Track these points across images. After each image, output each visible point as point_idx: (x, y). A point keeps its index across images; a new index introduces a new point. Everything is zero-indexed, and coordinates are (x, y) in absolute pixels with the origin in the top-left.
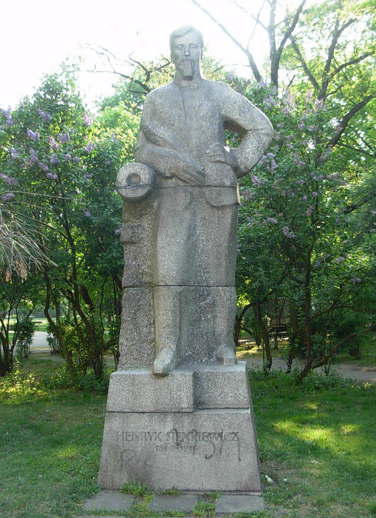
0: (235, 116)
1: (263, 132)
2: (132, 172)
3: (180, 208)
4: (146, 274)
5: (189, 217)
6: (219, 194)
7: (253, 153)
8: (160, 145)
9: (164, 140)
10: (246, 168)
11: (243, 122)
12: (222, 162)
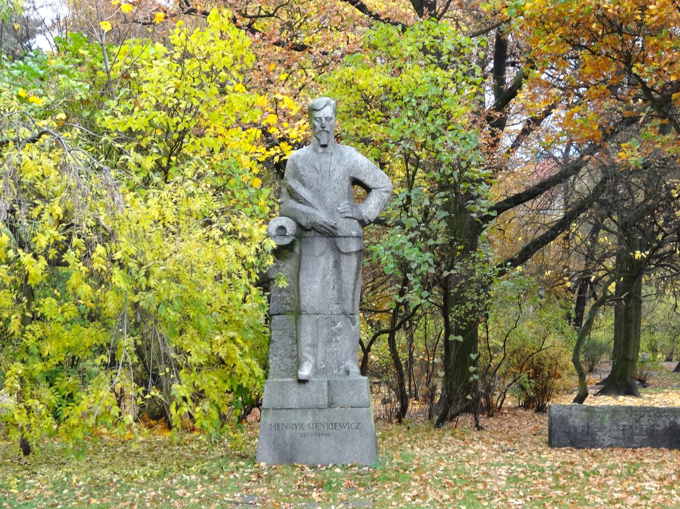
0: (361, 177)
1: (384, 189)
2: (280, 225)
3: (317, 254)
4: (289, 304)
5: (324, 261)
6: (347, 243)
7: (376, 208)
8: (301, 203)
9: (305, 199)
10: (369, 220)
11: (368, 181)
12: (350, 218)
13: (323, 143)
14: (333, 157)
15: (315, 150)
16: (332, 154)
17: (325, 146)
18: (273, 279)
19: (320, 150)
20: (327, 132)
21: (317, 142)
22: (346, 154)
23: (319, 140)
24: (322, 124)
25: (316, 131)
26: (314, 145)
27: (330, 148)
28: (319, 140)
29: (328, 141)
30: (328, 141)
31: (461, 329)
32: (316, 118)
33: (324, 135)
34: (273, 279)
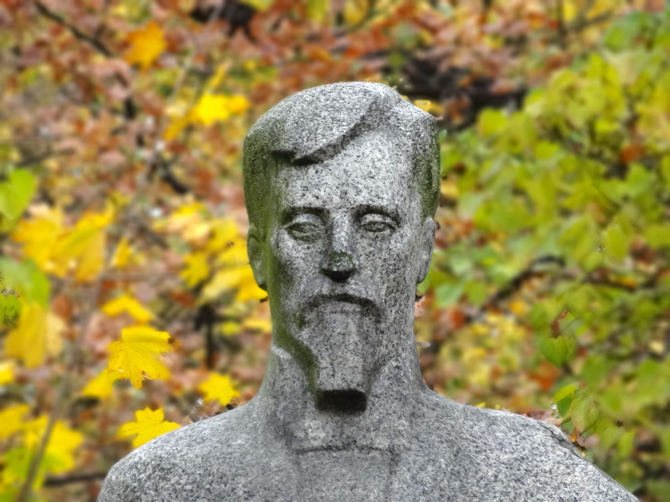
13: (331, 380)
14: (404, 474)
15: (284, 432)
16: (394, 457)
17: (346, 403)
18: (231, 33)
19: (316, 428)
20: (366, 305)
21: (293, 377)
22: (493, 462)
23: (306, 360)
24: (330, 254)
25: (293, 303)
26: (276, 395)
27: (382, 422)
28: (306, 360)
29: (373, 371)
30: (373, 371)
31: (261, 266)
32: (289, 215)
33: (345, 323)
34: (231, 33)
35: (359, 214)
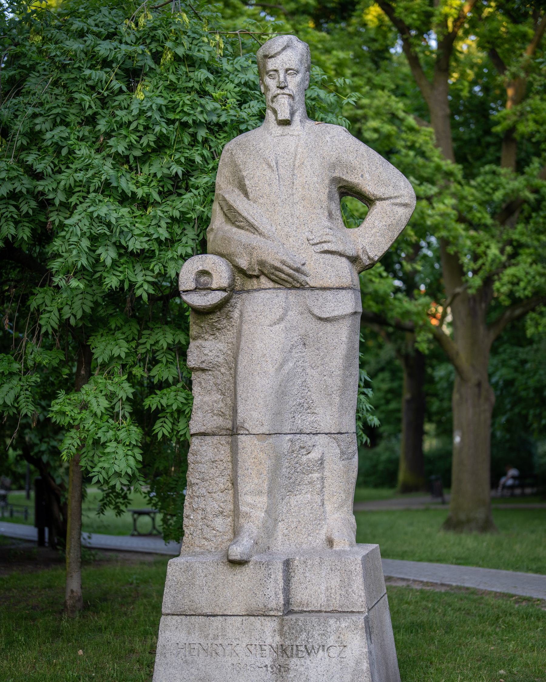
29: (292, 114)
35: (287, 70)
